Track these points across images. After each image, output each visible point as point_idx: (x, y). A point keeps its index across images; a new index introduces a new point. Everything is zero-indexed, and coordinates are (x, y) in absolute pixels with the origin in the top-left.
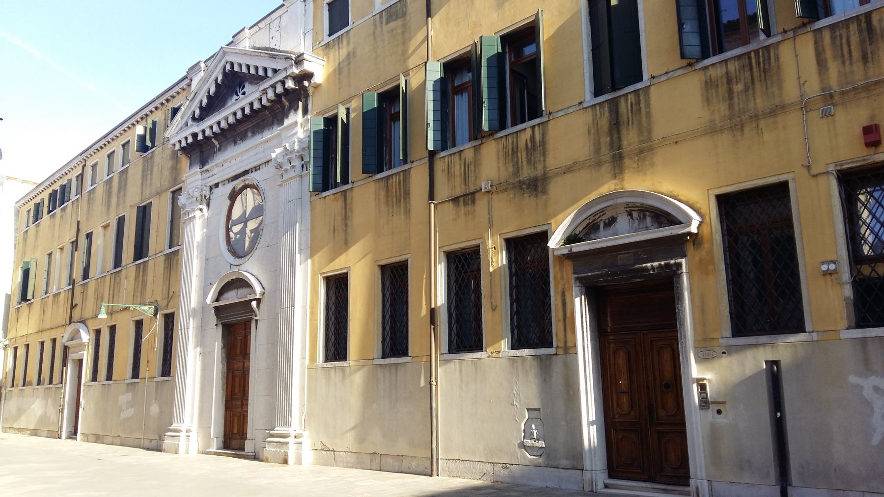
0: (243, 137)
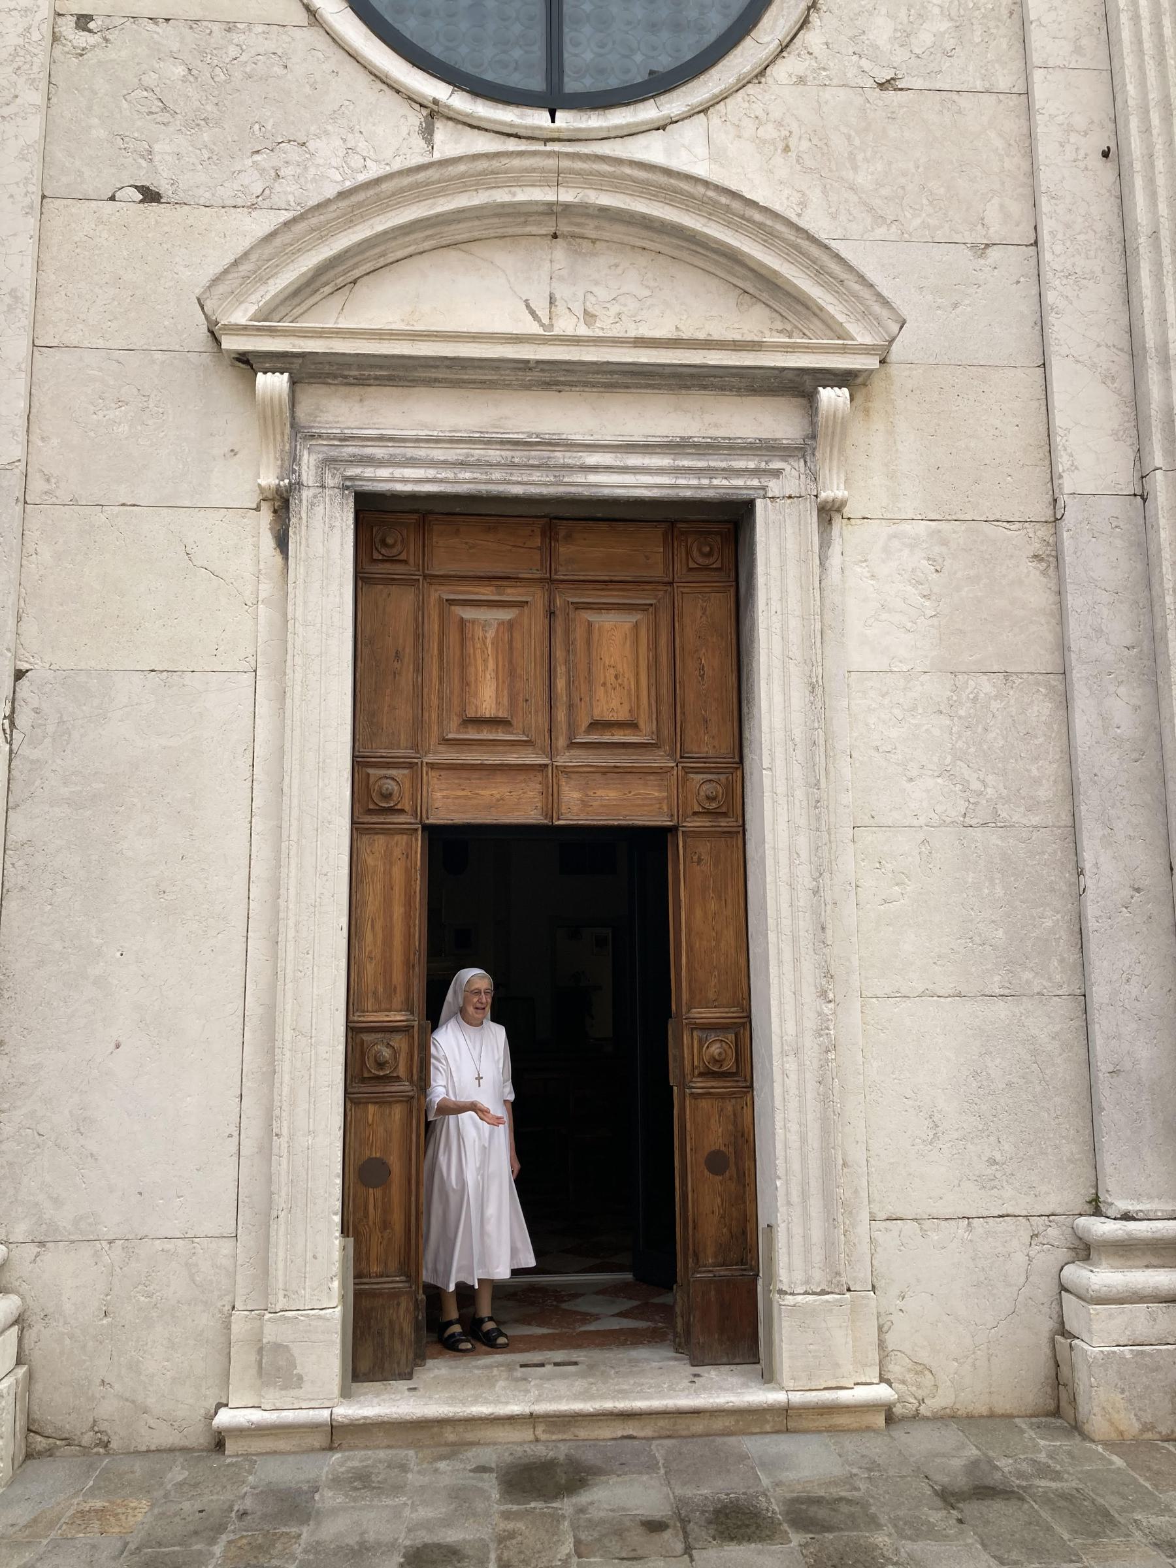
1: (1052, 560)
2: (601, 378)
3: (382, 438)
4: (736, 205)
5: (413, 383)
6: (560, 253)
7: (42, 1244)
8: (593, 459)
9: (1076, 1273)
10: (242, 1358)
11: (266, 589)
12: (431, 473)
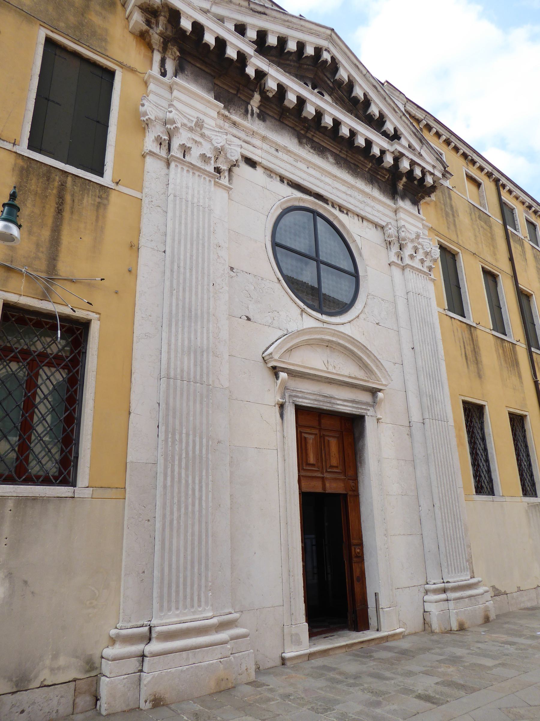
0: (320, 150)
1: (410, 435)
2: (339, 383)
3: (301, 391)
4: (364, 348)
5: (305, 378)
6: (328, 350)
7: (242, 612)
8: (339, 402)
9: (426, 598)
10: (287, 639)
11: (279, 428)
12: (309, 401)
